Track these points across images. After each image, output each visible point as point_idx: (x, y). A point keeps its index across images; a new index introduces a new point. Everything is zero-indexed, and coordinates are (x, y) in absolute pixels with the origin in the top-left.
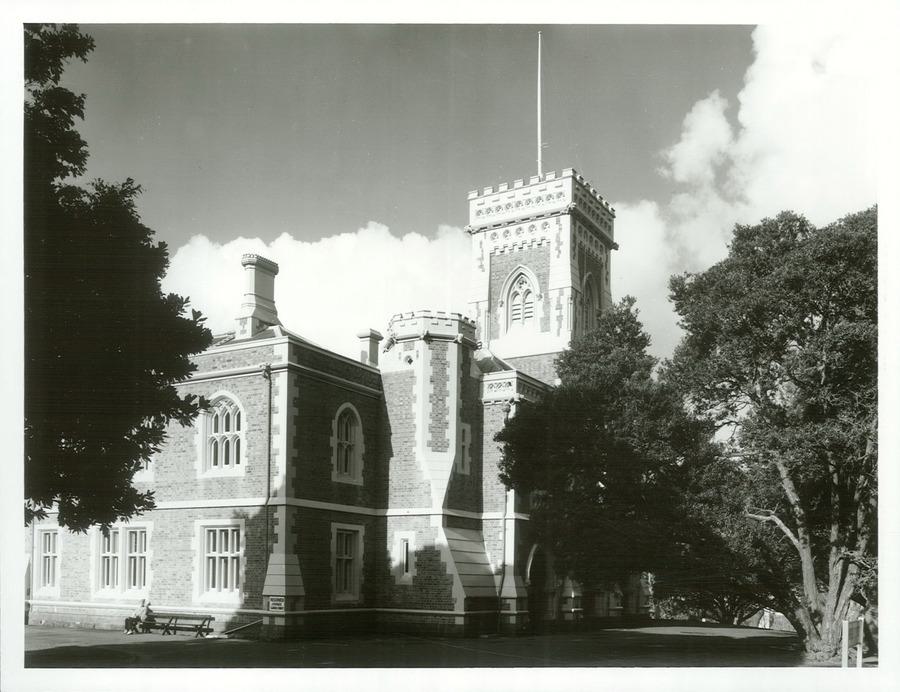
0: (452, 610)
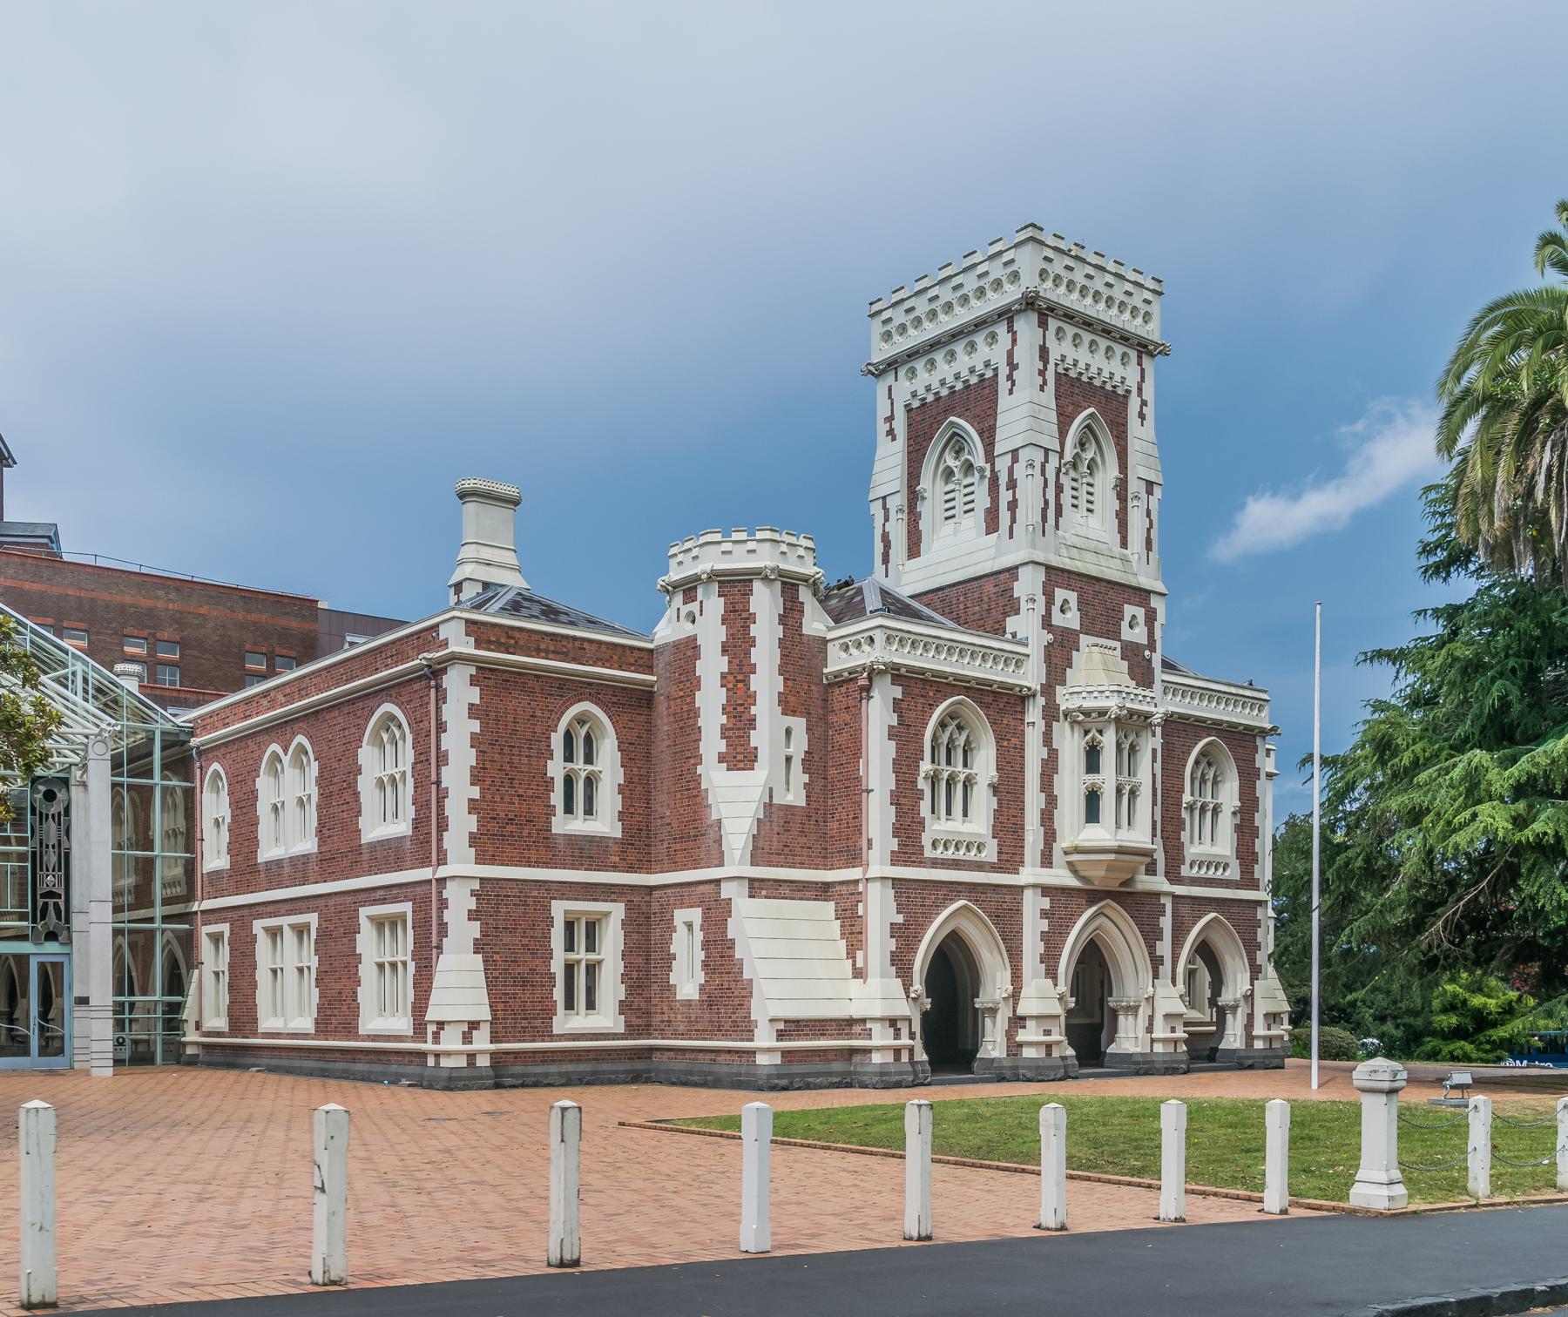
0: (752, 1040)
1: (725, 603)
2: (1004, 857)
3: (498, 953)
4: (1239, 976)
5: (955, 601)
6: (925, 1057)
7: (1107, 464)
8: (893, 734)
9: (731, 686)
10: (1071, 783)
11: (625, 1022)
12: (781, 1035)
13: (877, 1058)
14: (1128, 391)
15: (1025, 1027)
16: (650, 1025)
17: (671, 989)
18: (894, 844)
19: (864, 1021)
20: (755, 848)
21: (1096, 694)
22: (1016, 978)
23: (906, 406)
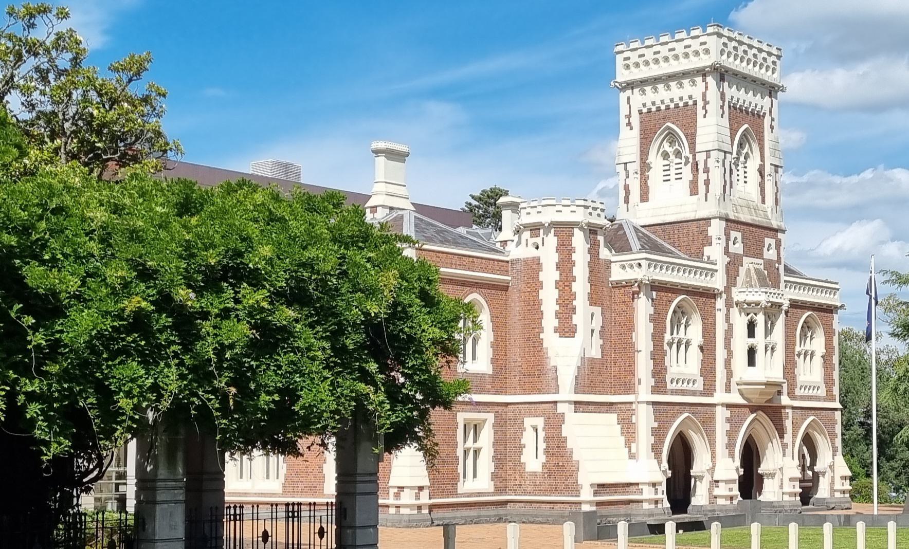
2: (706, 387)
4: (826, 454)
5: (672, 233)
6: (669, 505)
7: (754, 153)
9: (561, 288)
10: (741, 342)
13: (646, 506)
14: (764, 114)
15: (718, 487)
16: (506, 487)
17: (519, 464)
18: (652, 382)
19: (638, 484)
20: (577, 384)
21: (753, 293)
22: (713, 457)
23: (639, 111)
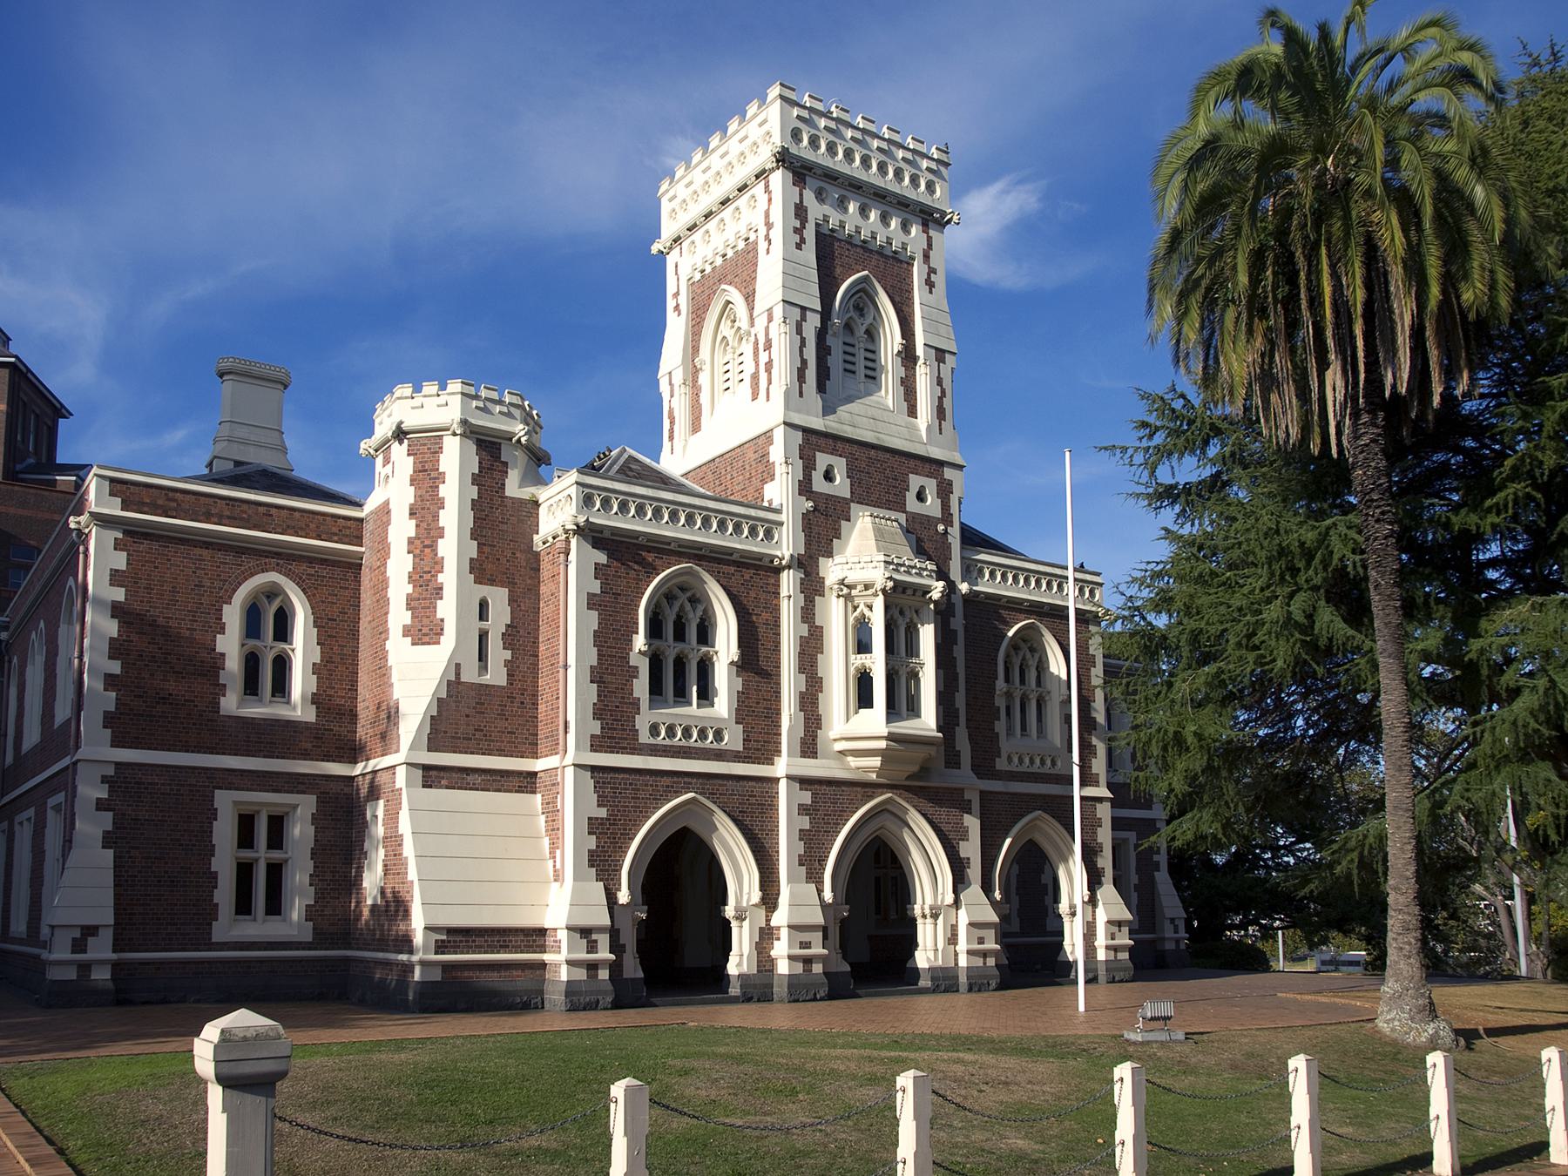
1: (415, 463)
3: (138, 848)
8: (592, 602)
11: (314, 929)
12: (440, 948)
